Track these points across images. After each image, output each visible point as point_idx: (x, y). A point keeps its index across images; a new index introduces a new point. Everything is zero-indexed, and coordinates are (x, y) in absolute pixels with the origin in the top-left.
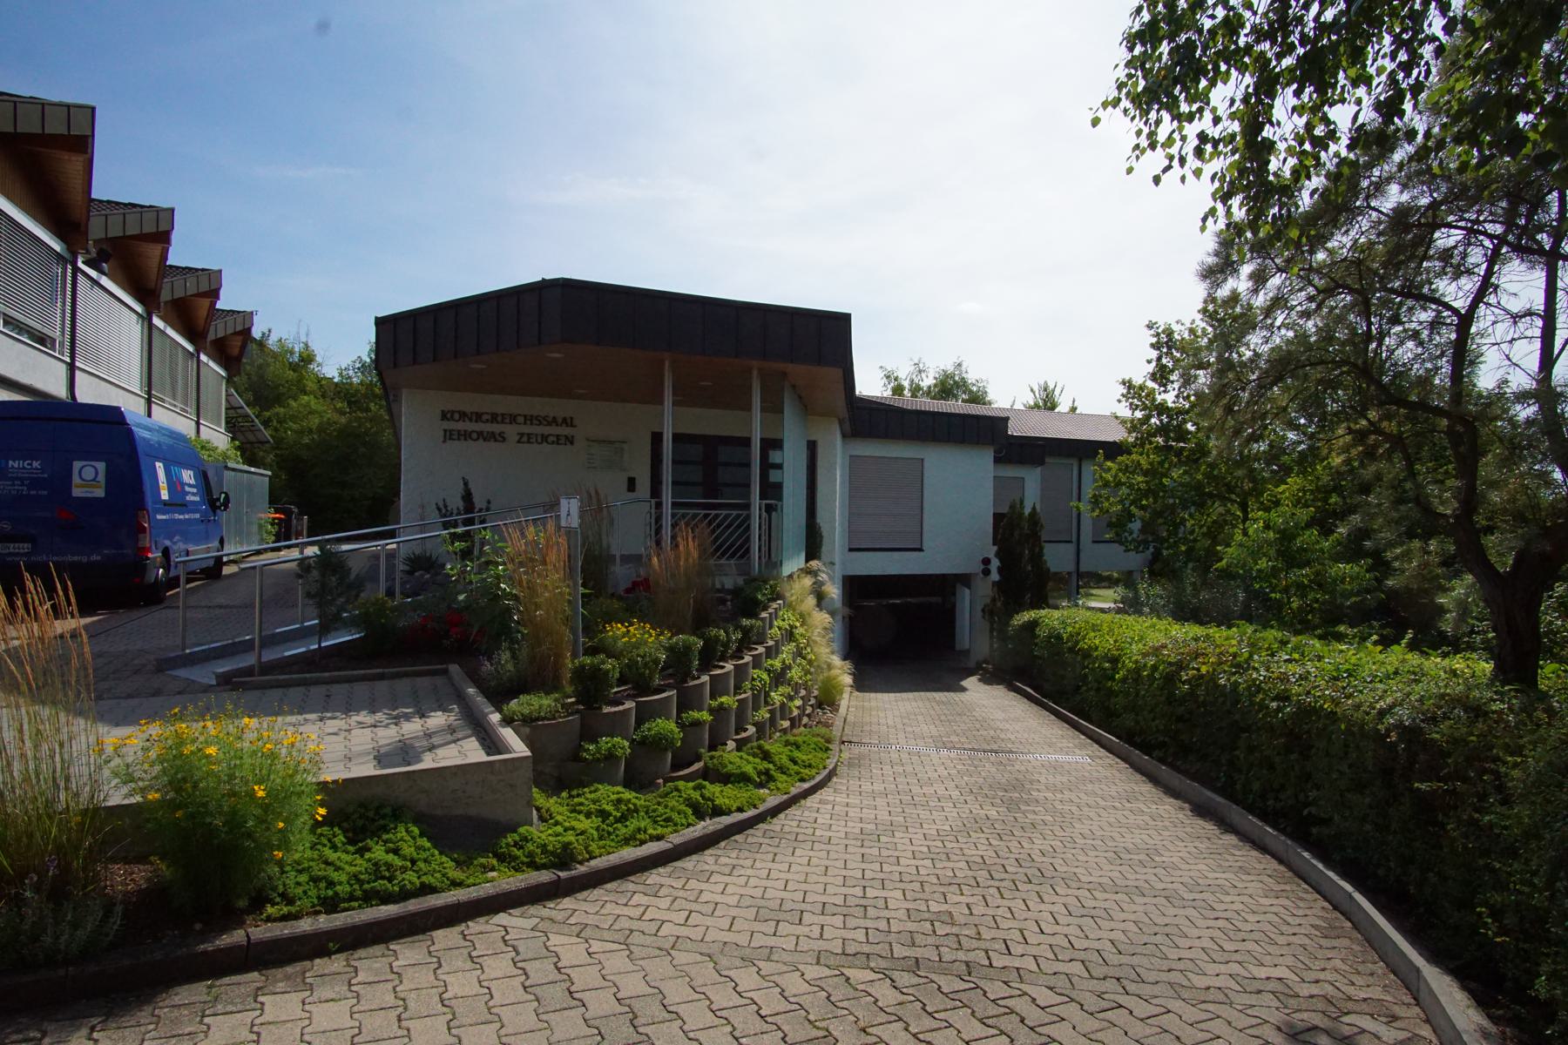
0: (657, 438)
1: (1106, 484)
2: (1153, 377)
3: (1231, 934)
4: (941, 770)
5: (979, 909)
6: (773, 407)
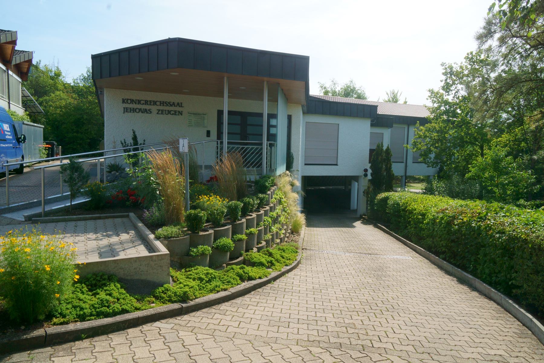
0: (220, 113)
1: (420, 137)
2: (443, 88)
3: (478, 335)
4: (346, 262)
5: (366, 322)
6: (273, 100)
